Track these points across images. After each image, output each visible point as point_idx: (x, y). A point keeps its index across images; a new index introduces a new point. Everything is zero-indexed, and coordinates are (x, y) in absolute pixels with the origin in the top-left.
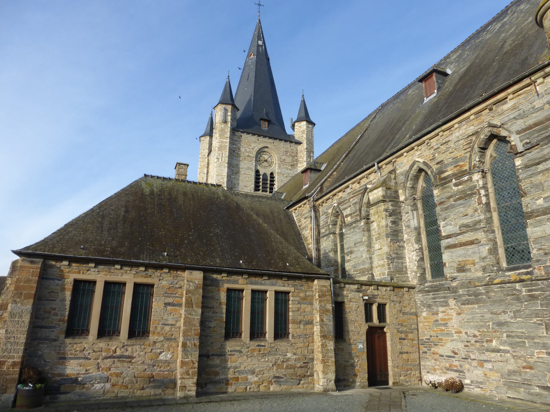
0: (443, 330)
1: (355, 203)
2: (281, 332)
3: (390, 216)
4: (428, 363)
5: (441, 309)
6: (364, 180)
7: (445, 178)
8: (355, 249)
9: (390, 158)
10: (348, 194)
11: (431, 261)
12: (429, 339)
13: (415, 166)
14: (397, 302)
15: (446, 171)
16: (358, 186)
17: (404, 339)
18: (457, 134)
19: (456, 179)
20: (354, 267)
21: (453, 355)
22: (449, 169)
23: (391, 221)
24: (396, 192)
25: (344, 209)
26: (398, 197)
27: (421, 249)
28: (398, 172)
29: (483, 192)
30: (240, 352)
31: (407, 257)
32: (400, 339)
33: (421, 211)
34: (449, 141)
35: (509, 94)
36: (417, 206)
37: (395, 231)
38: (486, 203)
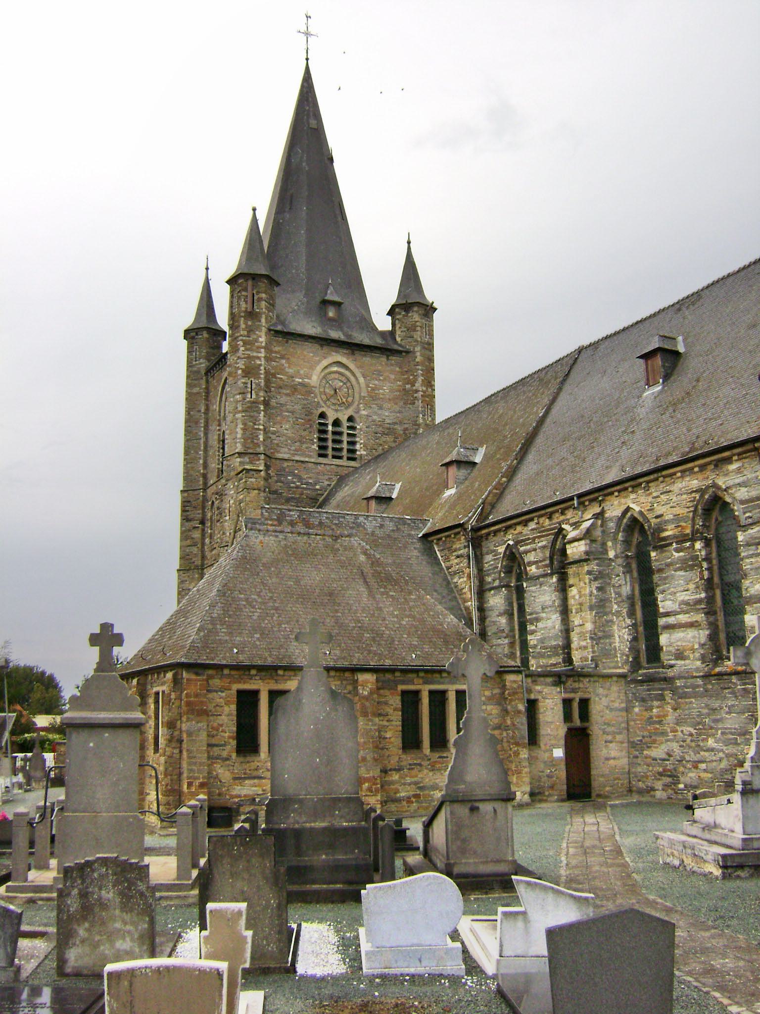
0: (657, 729)
1: (544, 547)
2: (439, 741)
3: (596, 579)
4: (639, 770)
5: (656, 703)
6: (557, 515)
7: (664, 539)
8: (544, 615)
9: (596, 495)
10: (532, 530)
11: (646, 641)
12: (641, 741)
13: (629, 514)
14: (603, 695)
15: (666, 530)
16: (547, 522)
17: (611, 742)
18: (680, 485)
19: (677, 543)
20: (542, 641)
21: (667, 757)
22: (669, 528)
23: (597, 588)
24: (604, 544)
25: (526, 552)
26: (606, 552)
27: (634, 625)
28: (607, 515)
29: (705, 565)
30: (420, 765)
31: (616, 635)
32: (606, 742)
33: (635, 574)
34: (670, 491)
35: (734, 455)
36: (630, 567)
37: (601, 600)
38: (708, 578)
